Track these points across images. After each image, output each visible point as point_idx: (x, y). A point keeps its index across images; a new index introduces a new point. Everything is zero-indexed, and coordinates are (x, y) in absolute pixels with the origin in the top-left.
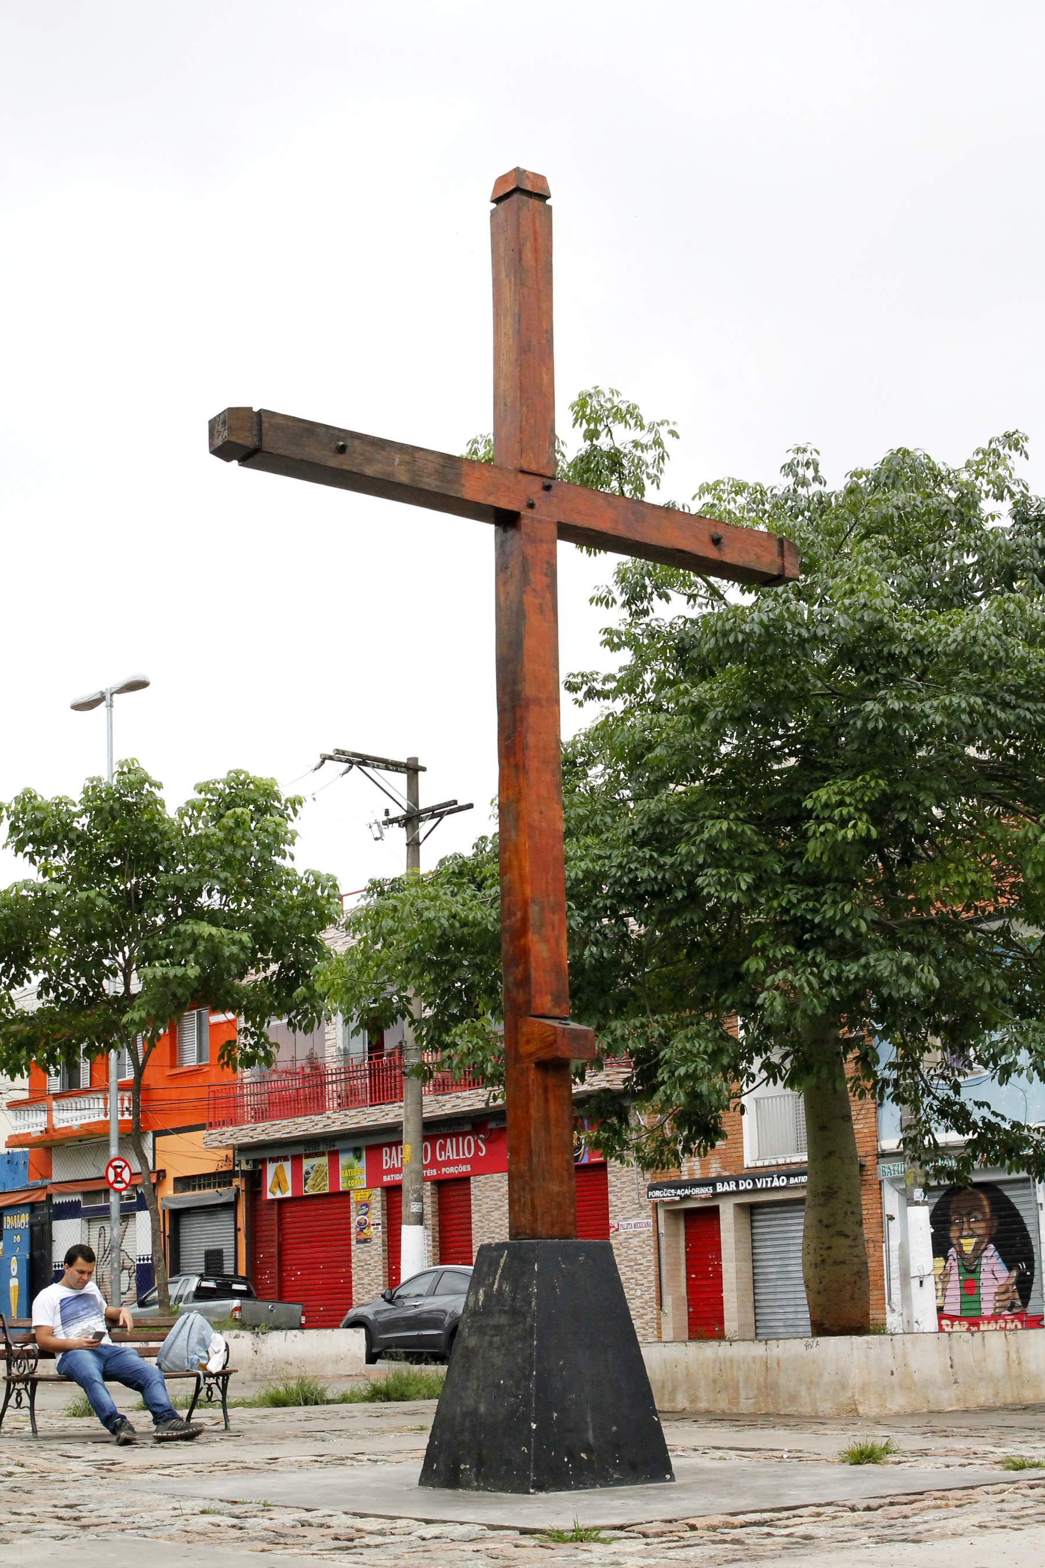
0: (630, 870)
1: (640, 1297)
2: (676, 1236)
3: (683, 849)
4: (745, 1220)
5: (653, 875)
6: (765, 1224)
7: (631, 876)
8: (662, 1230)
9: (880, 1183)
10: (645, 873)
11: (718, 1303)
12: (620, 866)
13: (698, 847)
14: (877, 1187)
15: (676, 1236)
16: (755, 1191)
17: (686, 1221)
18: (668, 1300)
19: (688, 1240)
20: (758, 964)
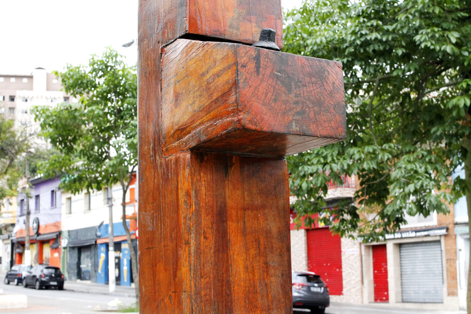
0: (362, 35)
1: (354, 280)
2: (369, 255)
3: (402, 17)
4: (397, 249)
5: (379, 37)
6: (406, 251)
7: (363, 39)
8: (363, 253)
9: (455, 236)
10: (374, 35)
11: (386, 283)
12: (354, 33)
13: (414, 16)
14: (454, 237)
15: (369, 255)
16: (402, 238)
17: (373, 252)
18: (366, 281)
19: (374, 257)
20: (465, 101)
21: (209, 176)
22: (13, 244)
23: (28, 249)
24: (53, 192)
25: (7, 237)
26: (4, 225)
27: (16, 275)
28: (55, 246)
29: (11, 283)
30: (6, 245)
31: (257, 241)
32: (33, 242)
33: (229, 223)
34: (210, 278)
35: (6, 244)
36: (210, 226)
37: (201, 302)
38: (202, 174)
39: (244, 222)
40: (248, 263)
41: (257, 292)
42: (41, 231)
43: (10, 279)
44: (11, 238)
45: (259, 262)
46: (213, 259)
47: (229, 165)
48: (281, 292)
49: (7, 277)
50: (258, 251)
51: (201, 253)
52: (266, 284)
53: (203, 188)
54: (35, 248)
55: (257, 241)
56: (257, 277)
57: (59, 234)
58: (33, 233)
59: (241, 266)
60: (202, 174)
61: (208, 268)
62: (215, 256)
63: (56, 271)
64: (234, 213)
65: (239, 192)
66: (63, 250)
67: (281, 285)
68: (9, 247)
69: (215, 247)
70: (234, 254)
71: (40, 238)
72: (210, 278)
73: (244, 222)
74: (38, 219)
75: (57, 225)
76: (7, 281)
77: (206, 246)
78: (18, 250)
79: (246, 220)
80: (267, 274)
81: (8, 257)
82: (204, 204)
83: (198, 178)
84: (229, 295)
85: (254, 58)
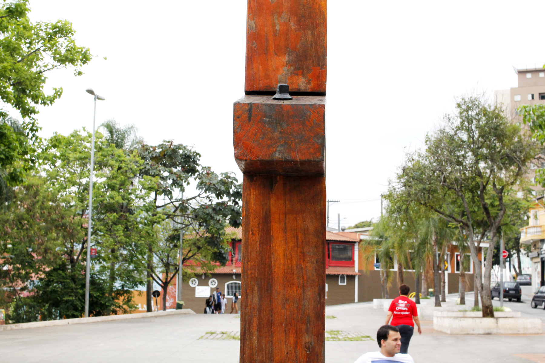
21: (257, 191)
25: (537, 255)
26: (532, 241)
29: (538, 307)
30: (536, 264)
31: (296, 237)
33: (272, 224)
34: (255, 262)
35: (535, 263)
36: (257, 226)
37: (248, 278)
38: (252, 190)
39: (285, 224)
40: (287, 252)
41: (294, 273)
43: (537, 302)
44: (541, 256)
45: (297, 252)
46: (258, 249)
47: (274, 182)
48: (315, 274)
49: (533, 299)
50: (296, 244)
51: (249, 245)
52: (302, 268)
53: (252, 200)
55: (296, 237)
56: (294, 262)
59: (281, 255)
60: (252, 190)
61: (254, 255)
62: (260, 247)
64: (277, 216)
65: (281, 202)
67: (316, 269)
69: (260, 241)
70: (275, 246)
72: (255, 262)
73: (285, 224)
76: (533, 304)
77: (253, 240)
79: (287, 221)
80: (304, 261)
81: (538, 277)
82: (253, 211)
83: (249, 192)
85: (247, 111)
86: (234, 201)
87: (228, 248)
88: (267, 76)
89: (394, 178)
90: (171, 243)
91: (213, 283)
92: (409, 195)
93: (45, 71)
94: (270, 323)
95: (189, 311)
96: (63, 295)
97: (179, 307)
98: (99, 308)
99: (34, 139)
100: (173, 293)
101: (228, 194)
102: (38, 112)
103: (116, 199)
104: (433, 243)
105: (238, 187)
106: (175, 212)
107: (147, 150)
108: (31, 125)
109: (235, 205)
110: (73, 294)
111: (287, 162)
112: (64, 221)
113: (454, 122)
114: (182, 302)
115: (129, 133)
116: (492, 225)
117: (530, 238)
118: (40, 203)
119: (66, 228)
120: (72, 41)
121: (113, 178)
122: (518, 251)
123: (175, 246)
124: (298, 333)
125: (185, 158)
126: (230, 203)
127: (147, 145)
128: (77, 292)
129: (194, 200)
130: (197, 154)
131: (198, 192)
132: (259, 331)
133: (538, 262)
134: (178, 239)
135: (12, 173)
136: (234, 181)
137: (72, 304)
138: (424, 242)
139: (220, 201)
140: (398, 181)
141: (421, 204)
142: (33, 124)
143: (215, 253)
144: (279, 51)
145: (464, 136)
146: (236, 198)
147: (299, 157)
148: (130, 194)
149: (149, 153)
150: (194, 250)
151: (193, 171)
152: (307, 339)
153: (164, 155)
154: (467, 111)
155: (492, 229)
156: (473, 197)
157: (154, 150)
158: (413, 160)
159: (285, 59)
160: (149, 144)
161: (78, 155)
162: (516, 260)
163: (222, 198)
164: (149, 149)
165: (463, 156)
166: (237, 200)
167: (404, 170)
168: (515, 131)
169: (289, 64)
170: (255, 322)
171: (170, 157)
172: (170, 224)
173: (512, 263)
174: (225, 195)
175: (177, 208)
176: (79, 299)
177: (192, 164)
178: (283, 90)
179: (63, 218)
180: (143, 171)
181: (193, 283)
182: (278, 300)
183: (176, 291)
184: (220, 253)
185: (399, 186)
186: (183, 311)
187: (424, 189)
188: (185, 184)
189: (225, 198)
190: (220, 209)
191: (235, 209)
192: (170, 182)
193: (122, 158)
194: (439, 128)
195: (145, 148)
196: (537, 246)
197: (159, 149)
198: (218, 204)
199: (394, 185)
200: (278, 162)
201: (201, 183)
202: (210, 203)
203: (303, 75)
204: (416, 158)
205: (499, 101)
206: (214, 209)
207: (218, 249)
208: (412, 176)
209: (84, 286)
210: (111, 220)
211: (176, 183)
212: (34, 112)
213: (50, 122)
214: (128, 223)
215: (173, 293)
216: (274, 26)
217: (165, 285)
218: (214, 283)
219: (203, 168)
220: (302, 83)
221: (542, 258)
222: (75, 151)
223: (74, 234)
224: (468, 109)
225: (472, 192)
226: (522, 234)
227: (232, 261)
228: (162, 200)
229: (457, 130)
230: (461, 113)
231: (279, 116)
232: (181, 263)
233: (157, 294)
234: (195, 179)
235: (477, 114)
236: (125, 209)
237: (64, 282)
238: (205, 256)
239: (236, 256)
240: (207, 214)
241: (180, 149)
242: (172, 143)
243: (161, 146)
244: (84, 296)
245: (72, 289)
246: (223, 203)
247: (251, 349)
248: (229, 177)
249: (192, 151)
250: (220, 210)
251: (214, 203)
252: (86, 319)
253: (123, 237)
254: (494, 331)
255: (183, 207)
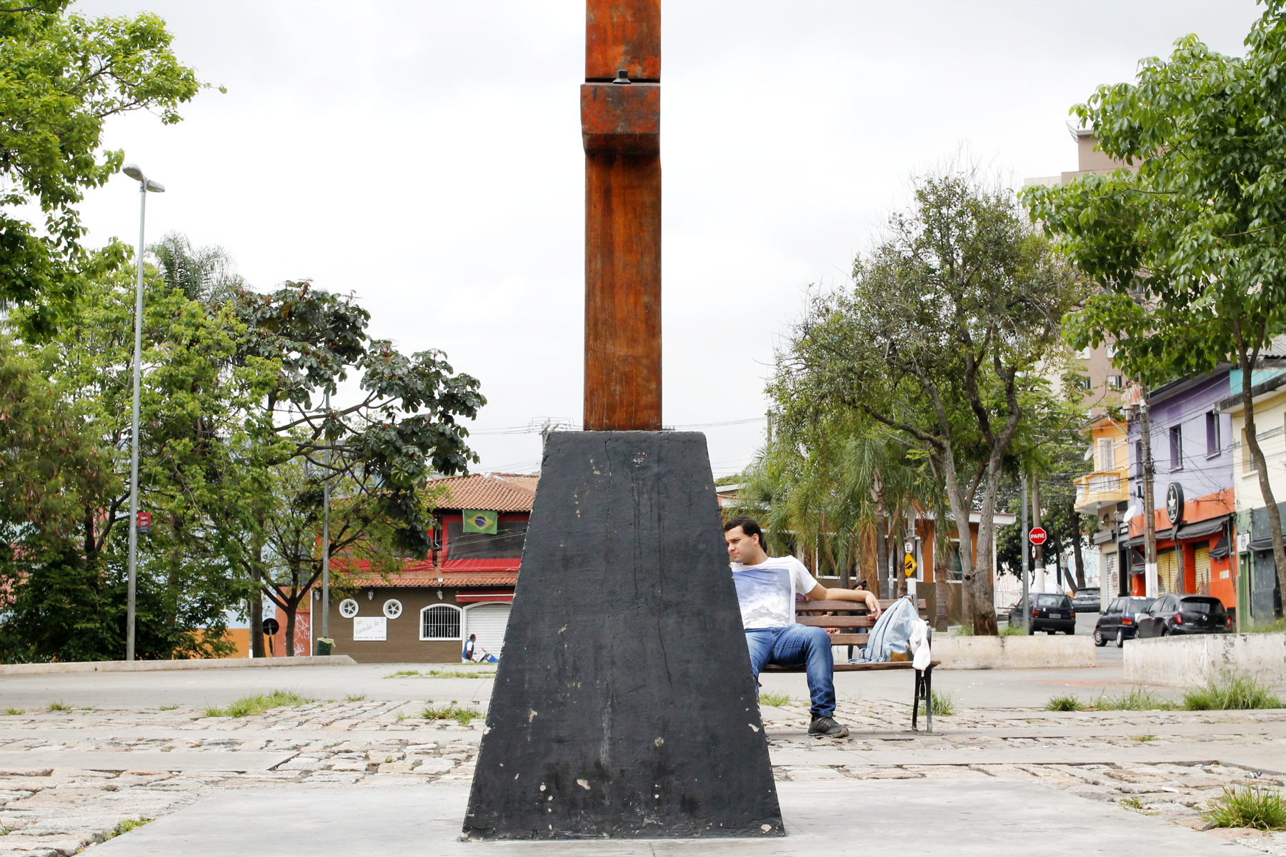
22: (1123, 553)
23: (1151, 561)
24: (1211, 417)
27: (1121, 620)
28: (1222, 551)
32: (1167, 545)
42: (1188, 518)
43: (1107, 634)
44: (1119, 539)
49: (1098, 627)
54: (1176, 559)
55: (635, 210)
57: (1229, 522)
58: (1166, 522)
63: (1212, 609)
66: (1240, 562)
68: (1116, 559)
71: (1186, 532)
74: (1178, 485)
75: (1224, 497)
76: (1099, 638)
78: (1135, 569)
84: (611, 243)
86: (443, 414)
87: (430, 523)
88: (606, 65)
89: (787, 349)
90: (303, 511)
91: (393, 609)
92: (819, 383)
93: (107, 114)
94: (612, 286)
95: (346, 657)
96: (75, 619)
97: (324, 650)
98: (155, 645)
99: (71, 250)
100: (302, 632)
101: (430, 402)
102: (82, 198)
103: (190, 407)
104: (875, 498)
105: (452, 384)
106: (315, 437)
107: (249, 304)
108: (66, 224)
109: (446, 423)
110: (95, 617)
111: (629, 136)
112: (79, 453)
113: (912, 229)
114: (328, 641)
115: (208, 268)
116: (993, 446)
117: (1096, 500)
118: (31, 412)
119: (84, 468)
120: (167, 58)
121: (180, 363)
122: (1077, 542)
123: (312, 518)
124: (637, 294)
125: (333, 322)
126: (435, 420)
127: (251, 294)
128: (105, 613)
129: (353, 415)
130: (362, 312)
131: (365, 394)
132: (602, 293)
133: (1115, 553)
134: (321, 503)
135: (36, 315)
136: (444, 372)
137: (92, 639)
138: (856, 498)
139: (411, 415)
140: (797, 355)
141: (844, 402)
142: (70, 221)
143: (401, 532)
144: (617, 41)
145: (934, 261)
146: (447, 408)
147: (638, 131)
148: (218, 397)
149: (255, 310)
150: (356, 526)
151: (351, 351)
152: (645, 299)
153: (290, 314)
154: (939, 207)
155: (993, 453)
156: (955, 388)
157: (268, 303)
158: (827, 310)
159: (623, 48)
160: (256, 292)
161: (102, 313)
162: (1072, 559)
163: (415, 410)
164: (256, 302)
165: (933, 301)
166: (451, 413)
167: (807, 329)
168: (1038, 249)
169: (626, 53)
170: (598, 285)
171: (303, 318)
172: (298, 468)
173: (1062, 564)
174: (423, 404)
175: (318, 432)
176: (109, 628)
177: (350, 335)
178: (623, 75)
179: (76, 447)
180: (245, 348)
181: (349, 607)
182: (619, 264)
183: (308, 629)
184: (413, 530)
185: (800, 366)
186: (332, 658)
187: (850, 370)
188: (336, 378)
189: (423, 410)
190: (413, 432)
191: (448, 432)
192: (305, 372)
193: (201, 320)
194: (880, 245)
195: (247, 300)
196: (1112, 518)
197: (277, 300)
198: (406, 422)
199: (787, 363)
200: (621, 136)
201: (373, 375)
202: (389, 421)
203: (640, 64)
204: (834, 306)
205: (1005, 186)
206: (400, 433)
207: (408, 521)
208: (825, 343)
209: (121, 598)
210: (179, 453)
211: (318, 374)
212: (73, 198)
213: (105, 216)
214: (216, 461)
215: (302, 632)
216: (612, 18)
217: (290, 606)
218: (393, 609)
219: (373, 343)
220: (638, 71)
221: (1121, 544)
222: (95, 304)
223: (100, 481)
224: (942, 202)
225: (952, 379)
226: (1079, 491)
227: (435, 558)
228: (284, 413)
229: (917, 249)
230: (925, 211)
231: (622, 97)
232: (326, 553)
233: (272, 625)
234: (358, 368)
235: (961, 214)
236: (201, 434)
237: (75, 590)
238: (379, 540)
239: (445, 548)
240: (386, 442)
241: (325, 301)
242: (306, 288)
243: (281, 295)
244: (122, 620)
245: (94, 606)
246: (419, 420)
247: (595, 308)
248: (433, 362)
249: (350, 305)
250: (414, 433)
251: (398, 421)
252: (130, 663)
253: (206, 493)
254: (998, 663)
255: (333, 424)
